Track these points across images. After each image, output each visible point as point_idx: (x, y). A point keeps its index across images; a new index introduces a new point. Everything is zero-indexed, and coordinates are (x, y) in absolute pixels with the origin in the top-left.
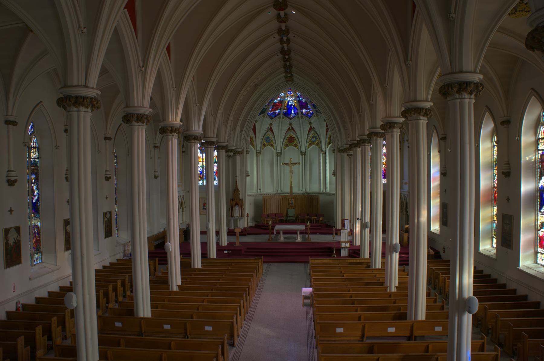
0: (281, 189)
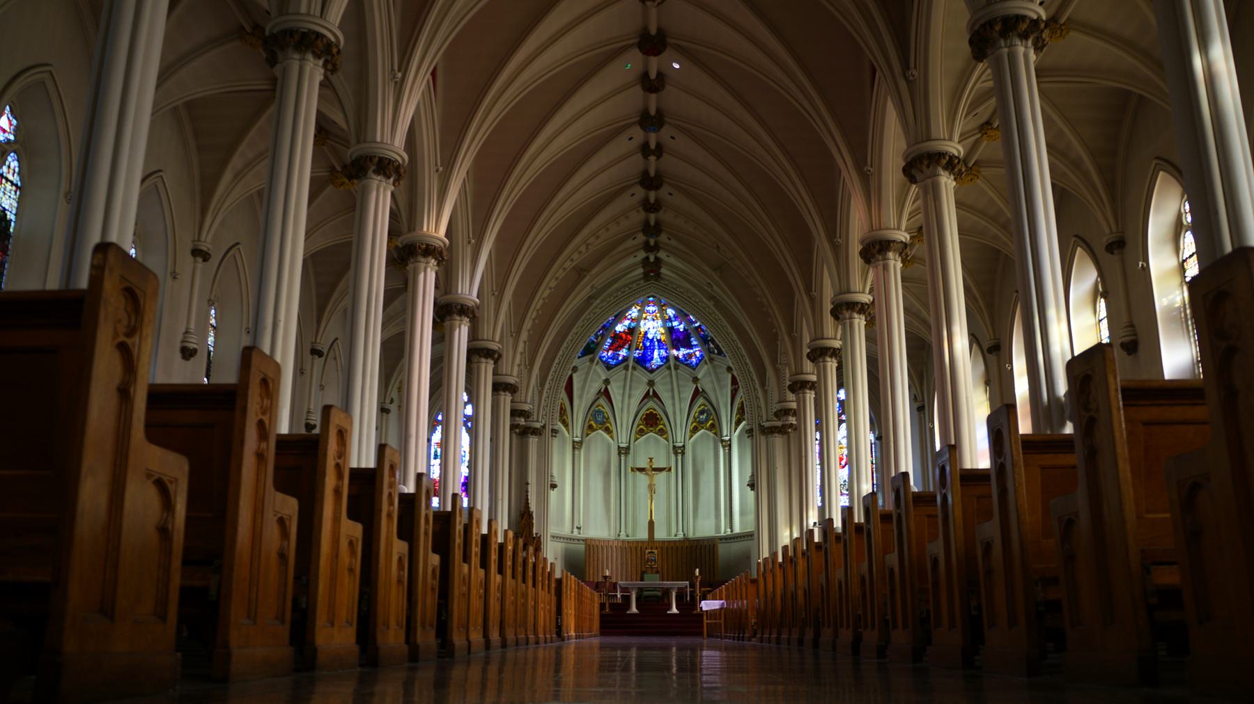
0: (626, 532)
